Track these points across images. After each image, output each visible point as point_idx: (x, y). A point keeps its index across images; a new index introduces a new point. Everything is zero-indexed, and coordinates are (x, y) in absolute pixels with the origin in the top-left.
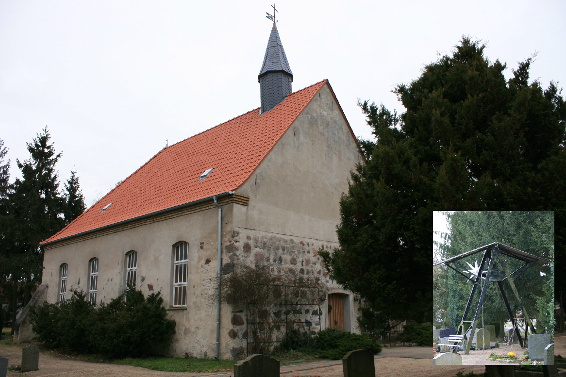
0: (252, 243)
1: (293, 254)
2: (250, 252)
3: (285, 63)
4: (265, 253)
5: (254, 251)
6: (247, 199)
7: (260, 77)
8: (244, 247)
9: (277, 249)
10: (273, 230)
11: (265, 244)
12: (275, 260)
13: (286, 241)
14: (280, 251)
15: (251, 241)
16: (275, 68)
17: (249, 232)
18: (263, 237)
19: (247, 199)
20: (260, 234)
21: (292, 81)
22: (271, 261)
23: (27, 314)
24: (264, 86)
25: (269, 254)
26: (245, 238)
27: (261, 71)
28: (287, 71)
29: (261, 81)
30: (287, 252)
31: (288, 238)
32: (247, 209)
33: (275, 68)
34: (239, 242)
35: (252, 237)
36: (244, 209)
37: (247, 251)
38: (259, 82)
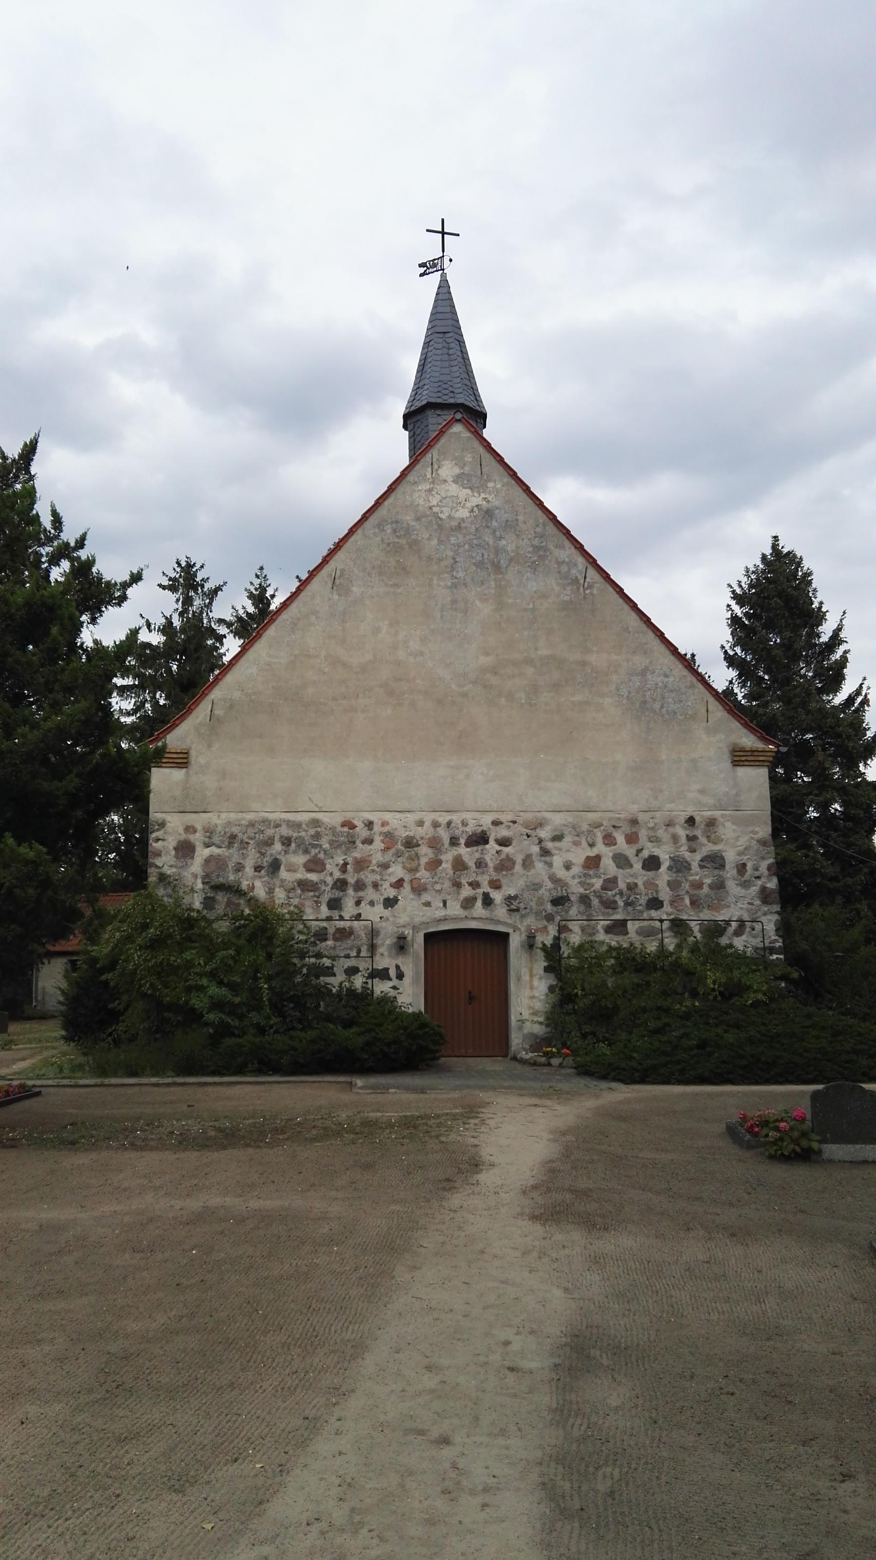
0: (197, 838)
1: (313, 852)
2: (193, 858)
3: (469, 383)
4: (233, 855)
5: (201, 853)
6: (185, 756)
7: (407, 417)
8: (175, 849)
9: (269, 842)
10: (256, 806)
11: (233, 837)
12: (258, 869)
13: (297, 826)
14: (278, 847)
15: (198, 835)
16: (446, 397)
17: (190, 819)
18: (229, 823)
19: (185, 756)
20: (218, 819)
21: (485, 427)
22: (249, 870)
23: (655, 1159)
24: (417, 440)
25: (244, 856)
26: (181, 830)
27: (412, 401)
28: (472, 405)
29: (410, 427)
30: (298, 846)
31: (304, 817)
32: (187, 773)
33: (446, 397)
34: (163, 840)
35: (199, 827)
36: (178, 775)
37: (185, 856)
38: (405, 427)
